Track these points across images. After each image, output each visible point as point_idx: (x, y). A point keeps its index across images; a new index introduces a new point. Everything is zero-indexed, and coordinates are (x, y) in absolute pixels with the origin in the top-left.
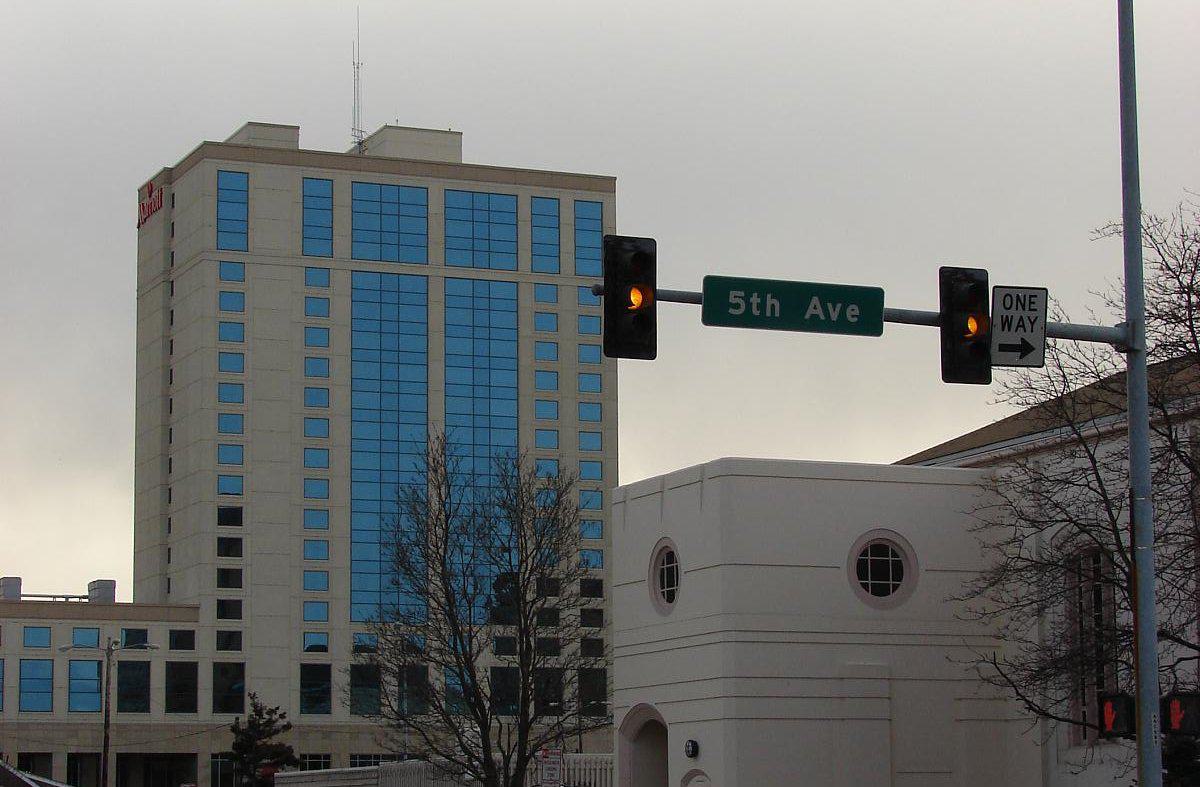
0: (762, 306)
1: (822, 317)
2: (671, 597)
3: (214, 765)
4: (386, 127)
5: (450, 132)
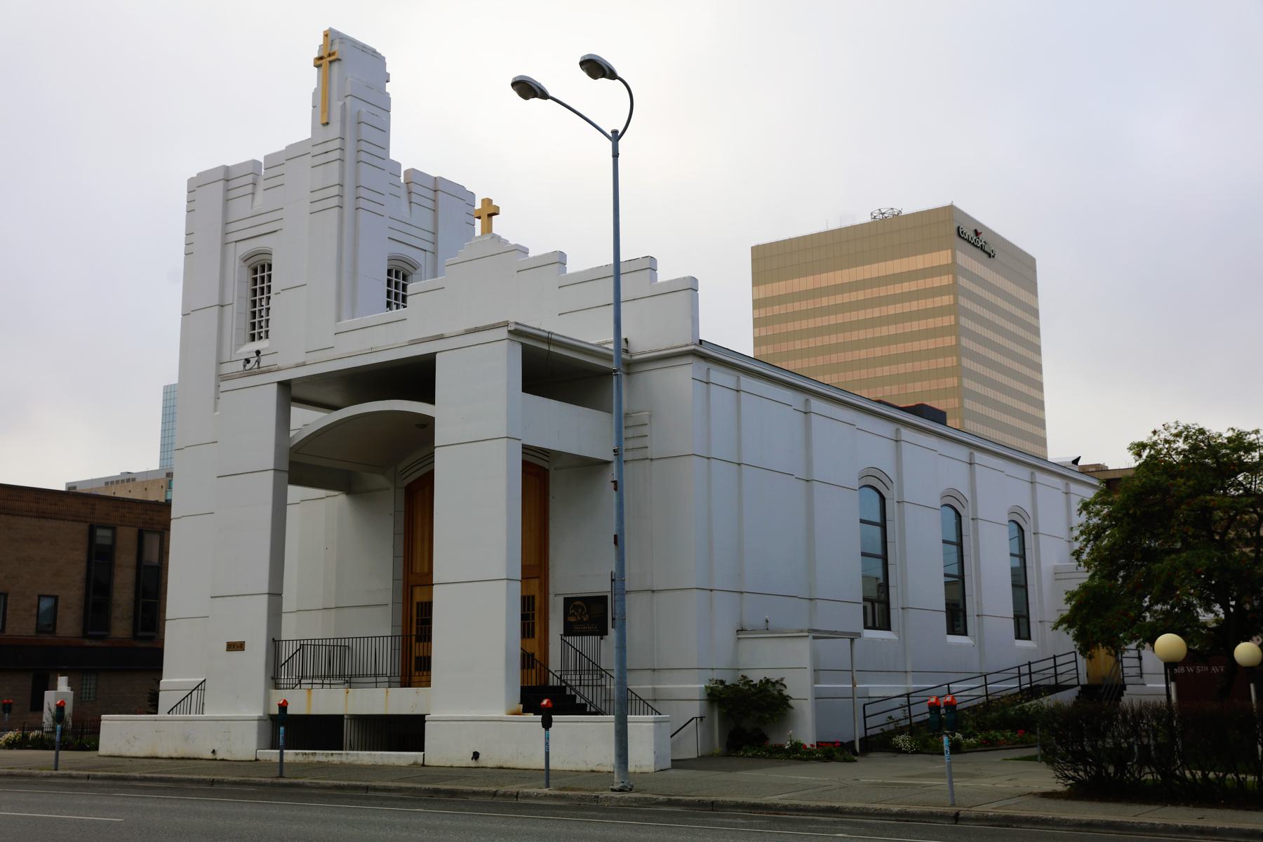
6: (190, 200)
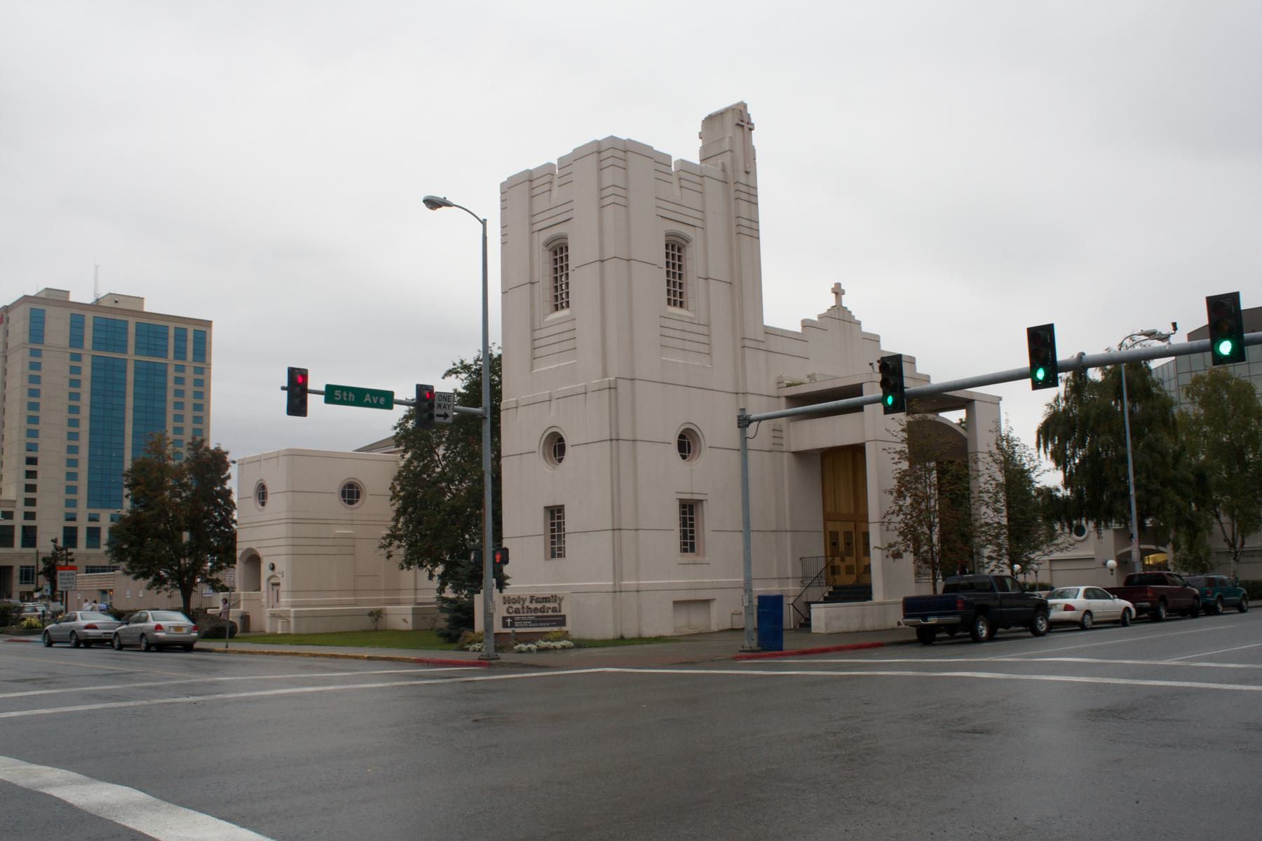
0: (347, 397)
1: (371, 402)
2: (263, 504)
3: (21, 571)
4: (110, 294)
5: (138, 298)
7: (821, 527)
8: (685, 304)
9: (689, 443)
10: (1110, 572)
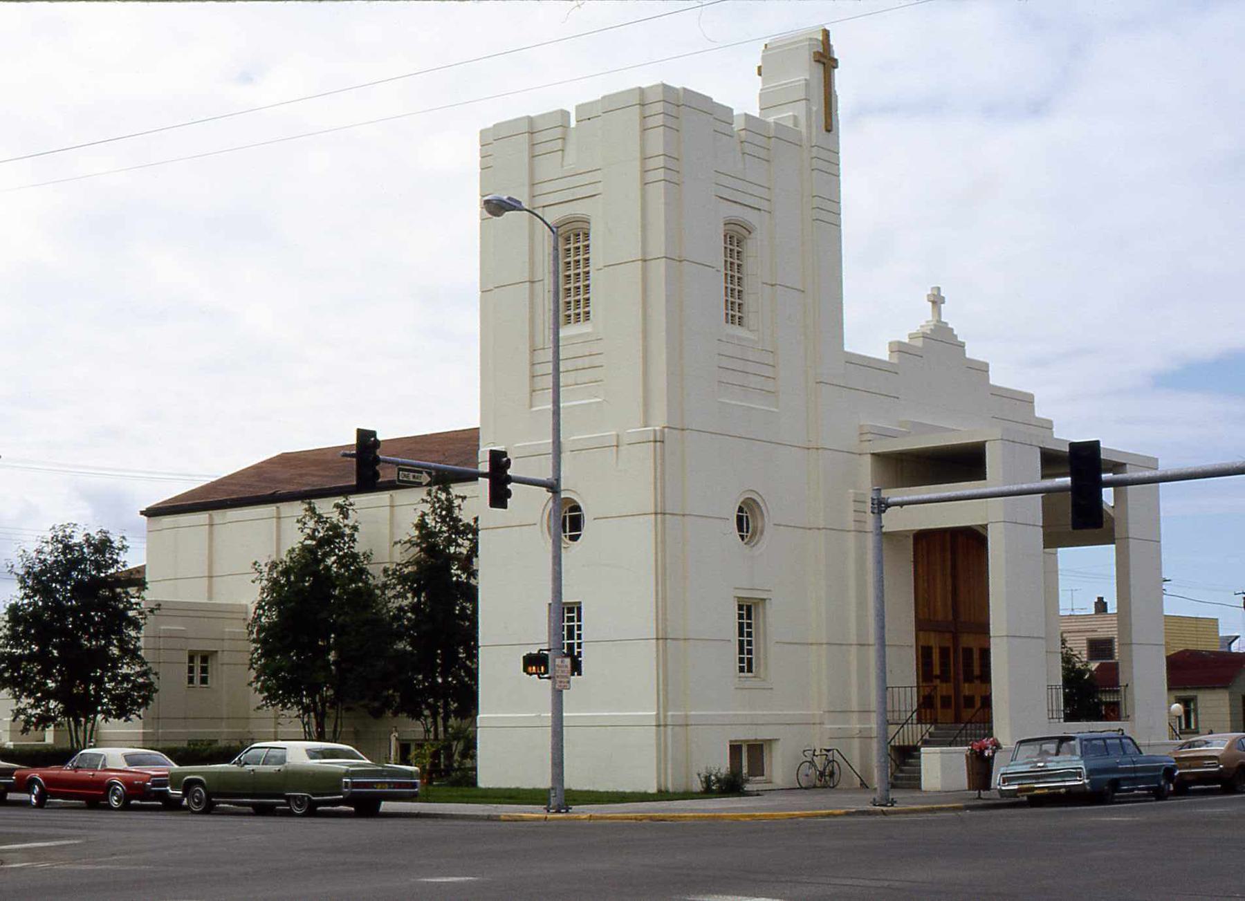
6: (483, 155)
7: (912, 641)
8: (745, 320)
9: (747, 517)
10: (51, 527)
